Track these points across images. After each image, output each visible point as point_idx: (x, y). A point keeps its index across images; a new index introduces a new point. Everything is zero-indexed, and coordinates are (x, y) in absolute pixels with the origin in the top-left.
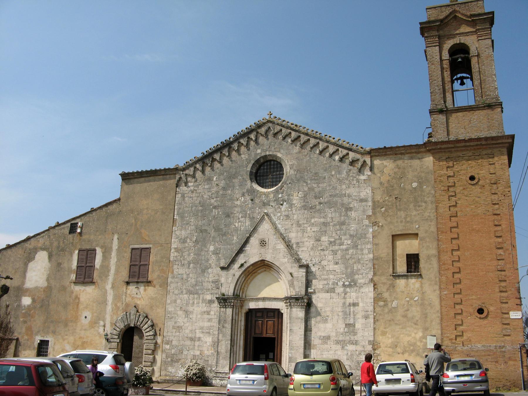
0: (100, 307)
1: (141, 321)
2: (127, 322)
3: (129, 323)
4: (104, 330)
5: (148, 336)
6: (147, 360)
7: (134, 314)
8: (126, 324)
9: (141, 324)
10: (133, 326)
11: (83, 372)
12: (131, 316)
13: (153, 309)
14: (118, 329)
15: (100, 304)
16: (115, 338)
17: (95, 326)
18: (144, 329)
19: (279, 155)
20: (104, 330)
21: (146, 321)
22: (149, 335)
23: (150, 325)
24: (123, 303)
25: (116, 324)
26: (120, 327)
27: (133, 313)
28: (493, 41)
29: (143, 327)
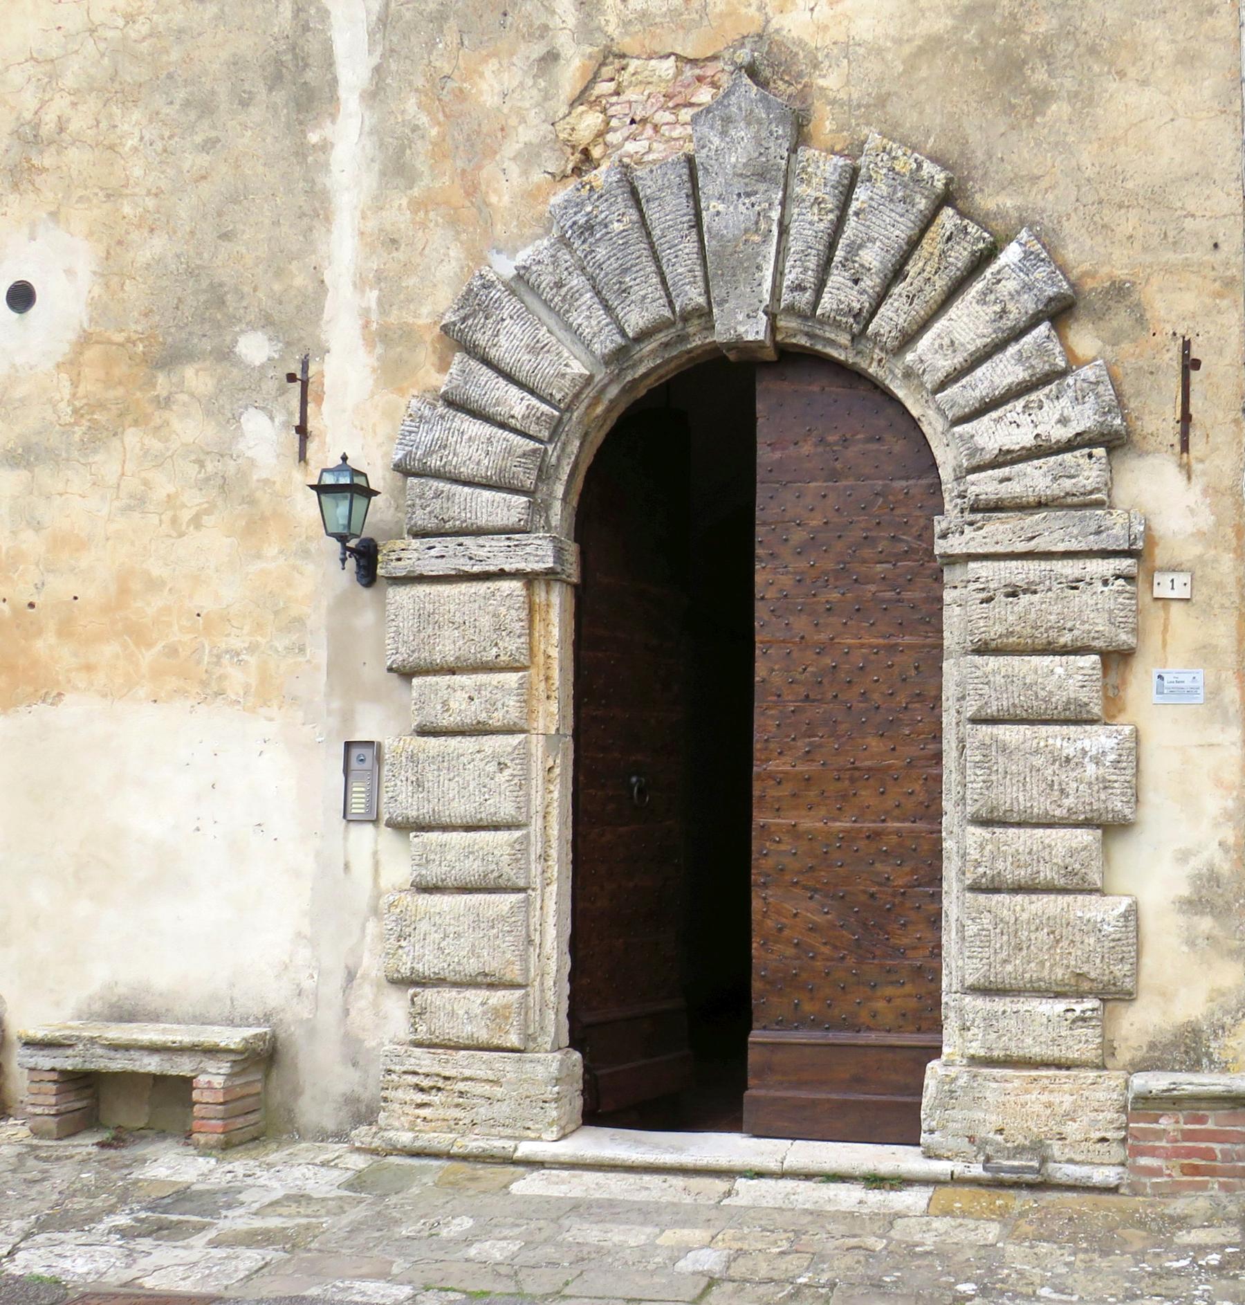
0: (209, 145)
1: (872, 257)
2: (649, 287)
3: (694, 296)
4: (302, 430)
5: (1006, 458)
6: (1012, 797)
7: (762, 175)
8: (635, 320)
9: (881, 298)
10: (754, 330)
11: (1117, 442)
12: (711, 207)
13: (1043, 98)
14: (516, 403)
15: (205, 107)
16: (483, 521)
17: (165, 403)
18: (945, 364)
19: (134, 1037)
20: (302, 430)
21: (960, 256)
22: (1023, 438)
23: (1029, 304)
24: (551, 57)
25: (481, 339)
26: (543, 369)
27: (736, 158)
28: (345, 816)
29: (908, 339)
